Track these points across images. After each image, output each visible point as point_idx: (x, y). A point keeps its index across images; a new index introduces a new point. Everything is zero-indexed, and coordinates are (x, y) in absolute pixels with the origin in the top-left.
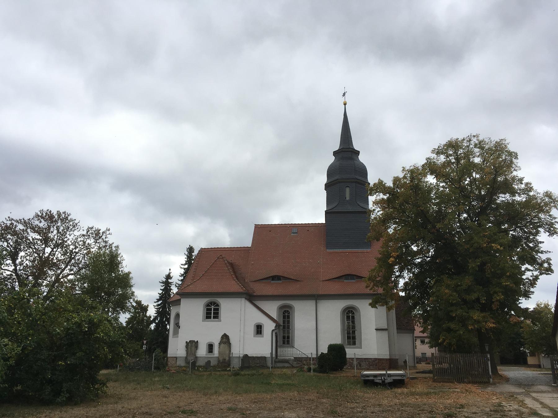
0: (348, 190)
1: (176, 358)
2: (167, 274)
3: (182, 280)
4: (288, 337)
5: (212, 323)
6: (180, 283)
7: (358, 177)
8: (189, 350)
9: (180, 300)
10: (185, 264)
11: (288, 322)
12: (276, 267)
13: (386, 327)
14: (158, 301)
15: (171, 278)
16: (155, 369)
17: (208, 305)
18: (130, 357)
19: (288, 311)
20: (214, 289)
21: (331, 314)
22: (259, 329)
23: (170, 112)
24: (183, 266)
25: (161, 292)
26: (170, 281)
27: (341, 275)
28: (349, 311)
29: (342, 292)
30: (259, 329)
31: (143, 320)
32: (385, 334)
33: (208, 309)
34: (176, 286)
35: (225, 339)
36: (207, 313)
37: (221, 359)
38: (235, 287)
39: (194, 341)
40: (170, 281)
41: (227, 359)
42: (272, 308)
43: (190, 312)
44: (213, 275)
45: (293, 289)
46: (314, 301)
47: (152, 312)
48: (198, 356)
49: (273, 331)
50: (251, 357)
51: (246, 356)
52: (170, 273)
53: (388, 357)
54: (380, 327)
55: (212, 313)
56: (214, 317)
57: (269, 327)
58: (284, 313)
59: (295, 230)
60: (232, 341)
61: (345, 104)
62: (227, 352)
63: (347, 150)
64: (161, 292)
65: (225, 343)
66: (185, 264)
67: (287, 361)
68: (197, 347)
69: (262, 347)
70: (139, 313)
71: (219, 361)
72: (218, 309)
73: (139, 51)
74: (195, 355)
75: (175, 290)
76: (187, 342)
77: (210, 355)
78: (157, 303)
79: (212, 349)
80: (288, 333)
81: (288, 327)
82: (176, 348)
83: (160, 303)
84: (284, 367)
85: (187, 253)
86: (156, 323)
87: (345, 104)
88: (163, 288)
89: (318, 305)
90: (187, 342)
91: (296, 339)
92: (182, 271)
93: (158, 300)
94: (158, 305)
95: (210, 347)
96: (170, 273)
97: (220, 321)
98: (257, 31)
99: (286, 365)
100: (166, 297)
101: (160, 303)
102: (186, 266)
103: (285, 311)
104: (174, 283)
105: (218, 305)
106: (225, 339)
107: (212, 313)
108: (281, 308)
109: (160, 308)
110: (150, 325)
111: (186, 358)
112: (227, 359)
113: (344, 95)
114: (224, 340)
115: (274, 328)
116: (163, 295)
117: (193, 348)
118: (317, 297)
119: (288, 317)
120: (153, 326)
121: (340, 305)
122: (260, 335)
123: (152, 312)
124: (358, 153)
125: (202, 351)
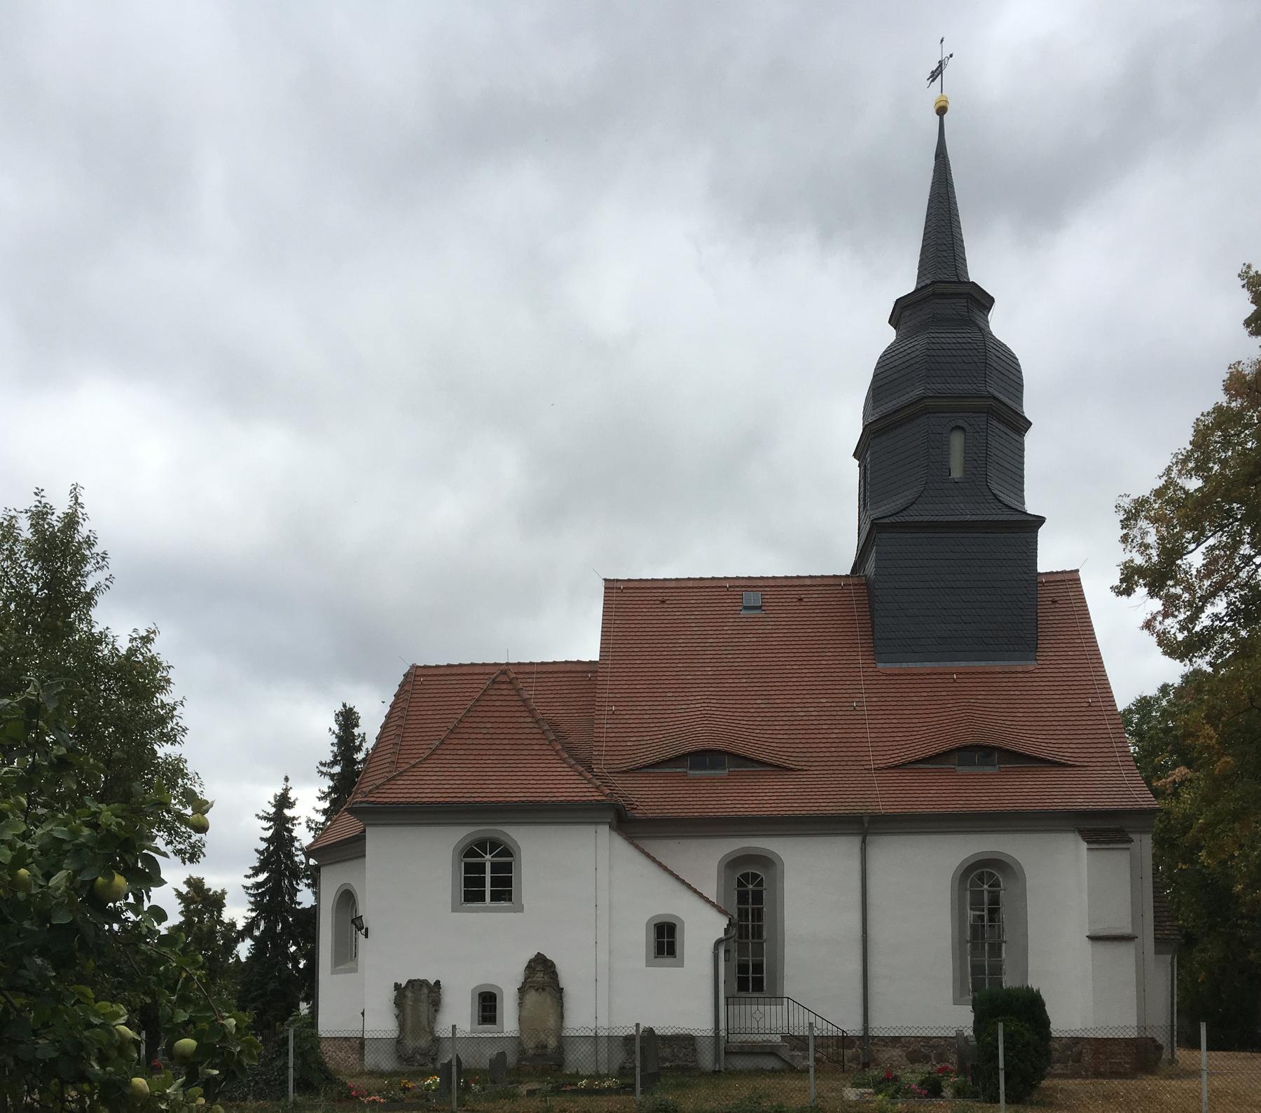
0: (957, 442)
1: (362, 1042)
2: (279, 791)
3: (325, 812)
4: (758, 968)
5: (487, 920)
6: (322, 819)
8: (408, 1010)
9: (360, 839)
10: (334, 763)
11: (758, 915)
12: (695, 720)
13: (1127, 930)
15: (291, 805)
16: (298, 1087)
17: (471, 854)
19: (755, 876)
21: (918, 881)
22: (665, 939)
24: (324, 769)
25: (263, 845)
27: (946, 747)
30: (665, 939)
31: (212, 932)
32: (1125, 956)
33: (469, 868)
35: (542, 976)
37: (530, 1045)
39: (424, 983)
41: (552, 1043)
42: (705, 861)
43: (408, 878)
44: (459, 758)
45: (766, 796)
47: (237, 912)
48: (566, 1033)
49: (718, 943)
51: (650, 1031)
52: (286, 790)
53: (1133, 1034)
54: (1101, 930)
55: (487, 879)
56: (496, 897)
57: (704, 928)
58: (740, 884)
59: (753, 598)
60: (565, 980)
61: (941, 111)
62: (552, 1023)
64: (263, 845)
65: (540, 988)
66: (334, 763)
67: (769, 1051)
68: (436, 1004)
69: (682, 1001)
70: (199, 913)
71: (522, 1052)
72: (508, 867)
74: (432, 1032)
77: (487, 1031)
79: (494, 1008)
81: (758, 933)
82: (352, 1004)
83: (262, 877)
84: (760, 1072)
85: (336, 728)
87: (941, 111)
88: (269, 834)
89: (872, 852)
95: (487, 1004)
96: (286, 790)
97: (520, 909)
98: (477, 127)
99: (769, 1063)
100: (279, 861)
101: (262, 877)
102: (337, 769)
103: (745, 876)
104: (303, 820)
105: (507, 852)
106: (542, 976)
107: (487, 879)
109: (262, 895)
111: (399, 1041)
112: (552, 1043)
113: (936, 74)
114: (540, 977)
116: (271, 855)
117: (424, 1007)
118: (865, 826)
119: (758, 897)
120: (244, 949)
121: (951, 853)
123: (237, 912)
125: (457, 1016)
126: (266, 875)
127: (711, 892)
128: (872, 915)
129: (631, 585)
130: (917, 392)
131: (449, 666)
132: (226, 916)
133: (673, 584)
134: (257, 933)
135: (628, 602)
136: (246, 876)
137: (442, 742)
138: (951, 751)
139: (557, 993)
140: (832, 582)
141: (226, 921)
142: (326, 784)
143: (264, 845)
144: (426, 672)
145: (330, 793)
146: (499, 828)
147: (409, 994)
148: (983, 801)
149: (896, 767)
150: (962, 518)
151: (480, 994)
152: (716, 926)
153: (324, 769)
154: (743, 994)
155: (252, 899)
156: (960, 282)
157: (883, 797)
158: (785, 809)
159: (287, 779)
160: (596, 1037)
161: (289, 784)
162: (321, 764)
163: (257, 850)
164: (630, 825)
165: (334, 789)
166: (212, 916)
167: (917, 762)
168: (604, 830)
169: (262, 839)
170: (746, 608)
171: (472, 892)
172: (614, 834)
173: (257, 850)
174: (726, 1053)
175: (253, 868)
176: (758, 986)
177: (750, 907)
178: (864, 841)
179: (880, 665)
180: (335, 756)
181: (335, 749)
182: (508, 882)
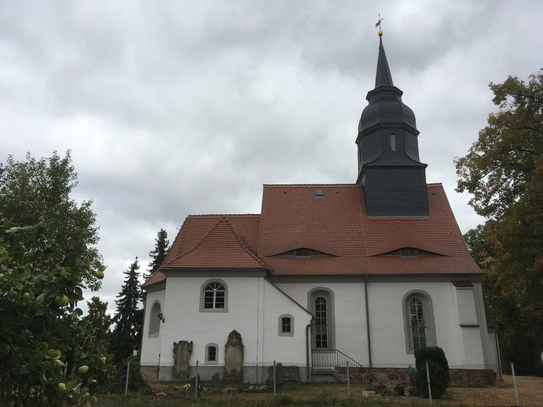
0: (393, 138)
1: (158, 368)
2: (133, 263)
3: (151, 271)
4: (325, 337)
5: (214, 316)
6: (149, 274)
7: (408, 124)
8: (179, 354)
9: (164, 282)
11: (324, 315)
12: (298, 237)
13: (476, 323)
14: (121, 296)
17: (208, 288)
18: (92, 389)
19: (323, 299)
20: (218, 263)
21: (389, 301)
22: (286, 325)
23: (132, 116)
24: (152, 254)
25: (125, 284)
26: (136, 271)
27: (397, 248)
28: (414, 300)
29: (402, 271)
30: (286, 325)
31: (100, 319)
32: (475, 334)
33: (207, 294)
34: (144, 278)
35: (235, 339)
36: (206, 300)
37: (229, 370)
38: (250, 263)
39: (186, 342)
40: (136, 271)
41: (238, 369)
42: (302, 292)
43: (182, 298)
44: (206, 252)
46: (363, 285)
47: (112, 311)
50: (286, 368)
52: (136, 262)
53: (483, 368)
55: (214, 299)
56: (218, 306)
57: (302, 320)
58: (316, 302)
59: (320, 192)
60: (245, 342)
61: (380, 35)
62: (238, 360)
63: (388, 89)
64: (125, 284)
65: (234, 345)
67: (330, 374)
69: (293, 351)
70: (96, 312)
71: (226, 373)
72: (223, 294)
73: (103, 47)
74: (188, 364)
75: (141, 281)
76: (175, 344)
77: (212, 364)
78: (119, 298)
80: (325, 330)
81: (324, 322)
82: (155, 352)
83: (123, 297)
84: (326, 383)
86: (117, 322)
87: (380, 35)
90: (175, 344)
91: (337, 339)
92: (152, 260)
93: (121, 295)
94: (121, 300)
95: (212, 352)
96: (136, 262)
97: (227, 311)
98: (221, 38)
99: (330, 379)
101: (123, 297)
102: (157, 254)
103: (319, 299)
104: (142, 274)
105: (223, 288)
106: (235, 339)
107: (214, 299)
108: (314, 293)
110: (110, 324)
111: (174, 368)
112: (238, 369)
114: (234, 340)
115: (309, 323)
117: (185, 353)
118: (366, 279)
119: (324, 307)
121: (403, 289)
122: (288, 333)
123: (112, 311)
124: (400, 93)
125: (199, 357)
126: (125, 296)
127: (305, 305)
128: (371, 315)
129: (273, 187)
131: (203, 215)
132: (107, 313)
133: (289, 187)
135: (271, 193)
137: (199, 244)
141: (107, 315)
143: (125, 284)
145: (153, 264)
147: (179, 347)
149: (377, 255)
151: (209, 348)
153: (152, 254)
154: (319, 348)
155: (118, 306)
157: (373, 268)
161: (138, 260)
162: (151, 252)
163: (122, 286)
164: (273, 277)
166: (101, 313)
170: (317, 195)
171: (208, 304)
172: (266, 281)
173: (122, 286)
174: (312, 374)
176: (325, 345)
177: (321, 312)
178: (366, 285)
179: (369, 217)
180: (157, 249)
182: (223, 300)
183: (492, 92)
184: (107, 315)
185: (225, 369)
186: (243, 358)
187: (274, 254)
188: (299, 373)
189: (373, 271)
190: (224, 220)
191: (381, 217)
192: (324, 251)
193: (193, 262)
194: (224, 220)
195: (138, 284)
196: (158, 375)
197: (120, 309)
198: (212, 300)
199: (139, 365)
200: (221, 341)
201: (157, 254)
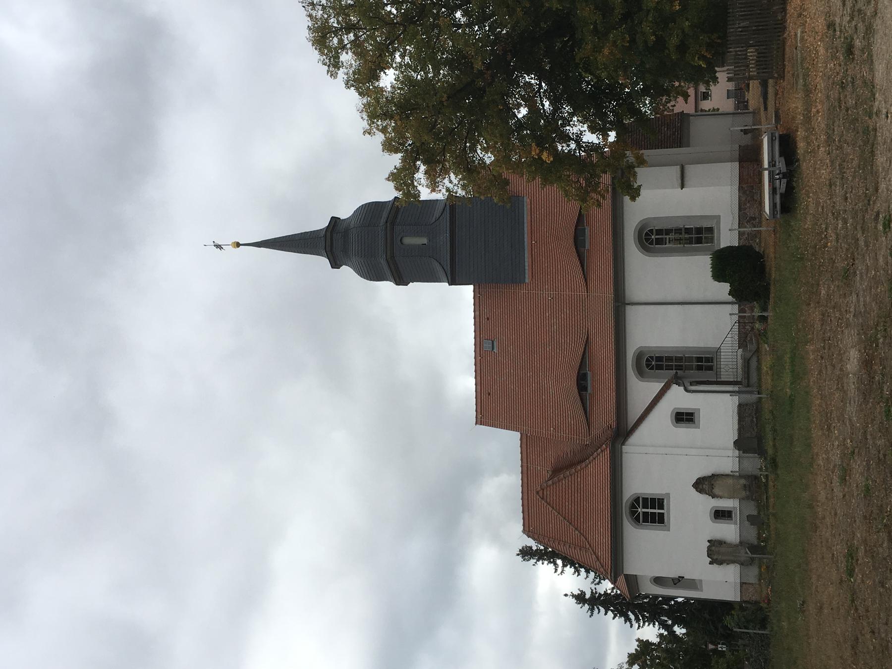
0: (408, 241)
2: (574, 601)
3: (587, 571)
4: (699, 359)
5: (674, 512)
6: (592, 575)
10: (555, 564)
11: (669, 359)
14: (630, 620)
17: (636, 519)
19: (647, 360)
20: (604, 505)
22: (684, 418)
24: (560, 569)
25: (610, 614)
26: (588, 596)
27: (575, 254)
29: (609, 254)
30: (684, 418)
31: (667, 650)
32: (690, 170)
34: (599, 583)
35: (704, 485)
37: (744, 494)
38: (602, 461)
39: (709, 549)
40: (588, 596)
41: (743, 481)
42: (641, 390)
43: (652, 555)
46: (628, 308)
49: (686, 390)
53: (737, 164)
55: (652, 511)
56: (661, 507)
57: (679, 398)
58: (652, 369)
59: (487, 345)
60: (707, 472)
61: (238, 245)
62: (730, 481)
64: (610, 614)
65: (712, 486)
66: (555, 564)
67: (747, 363)
69: (719, 411)
71: (747, 498)
72: (645, 500)
74: (736, 546)
75: (607, 586)
76: (711, 563)
77: (737, 515)
78: (634, 622)
80: (690, 359)
82: (722, 584)
83: (632, 617)
84: (759, 369)
85: (533, 561)
87: (238, 245)
88: (602, 610)
90: (711, 563)
91: (702, 345)
93: (627, 619)
94: (637, 620)
95: (720, 515)
97: (668, 495)
98: (89, 419)
99: (754, 363)
101: (632, 617)
103: (648, 366)
104: (593, 586)
105: (637, 500)
106: (704, 485)
107: (652, 511)
108: (641, 373)
109: (643, 616)
111: (742, 564)
112: (743, 481)
115: (682, 388)
117: (723, 549)
118: (620, 303)
119: (659, 359)
121: (635, 258)
124: (335, 221)
125: (729, 532)
126: (630, 613)
127: (656, 387)
128: (669, 299)
129: (479, 411)
130: (383, 262)
131: (523, 512)
132: (655, 640)
133: (479, 387)
134: (670, 622)
135: (489, 410)
136: (631, 626)
137: (576, 529)
138: (578, 252)
139: (714, 477)
140: (477, 300)
141: (658, 640)
142: (569, 570)
143: (610, 613)
144: (527, 525)
145: (575, 568)
146: (625, 500)
147: (715, 557)
148: (606, 239)
149: (586, 280)
150: (448, 239)
151: (715, 518)
152: (676, 391)
153: (560, 569)
154: (715, 368)
155: (647, 624)
156: (325, 235)
157: (604, 292)
158: (611, 346)
159: (566, 595)
160: (739, 457)
161: (569, 594)
162: (556, 571)
163: (614, 618)
164: (622, 432)
165: (572, 564)
166: (654, 649)
167: (582, 266)
168: (625, 448)
169: (606, 614)
170: (493, 349)
171: (659, 520)
172: (627, 443)
173: (614, 618)
174: (748, 386)
175: (626, 622)
176: (708, 360)
177: (664, 364)
178: (629, 304)
179: (527, 281)
180: (550, 562)
181: (546, 562)
182: (653, 500)
183: (391, 183)
184: (658, 640)
185: (743, 499)
186: (727, 475)
187: (585, 421)
188: (747, 405)
189: (609, 294)
190: (541, 493)
191: (526, 264)
192: (581, 352)
193: (602, 539)
194: (541, 493)
195: (609, 592)
196: (752, 584)
197: (651, 620)
198: (653, 507)
199: (740, 604)
200: (706, 504)
201: (559, 562)
